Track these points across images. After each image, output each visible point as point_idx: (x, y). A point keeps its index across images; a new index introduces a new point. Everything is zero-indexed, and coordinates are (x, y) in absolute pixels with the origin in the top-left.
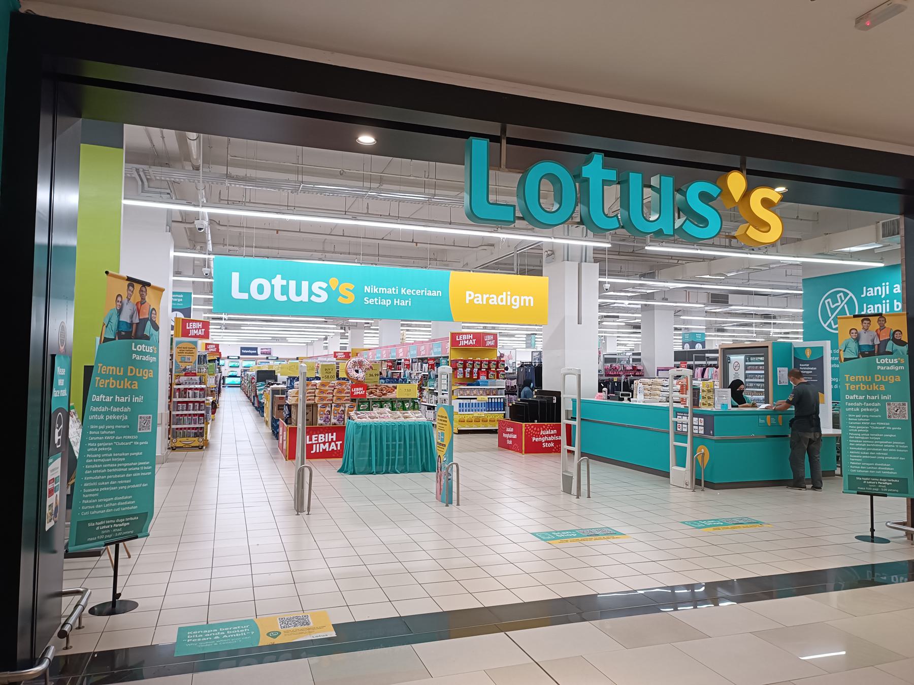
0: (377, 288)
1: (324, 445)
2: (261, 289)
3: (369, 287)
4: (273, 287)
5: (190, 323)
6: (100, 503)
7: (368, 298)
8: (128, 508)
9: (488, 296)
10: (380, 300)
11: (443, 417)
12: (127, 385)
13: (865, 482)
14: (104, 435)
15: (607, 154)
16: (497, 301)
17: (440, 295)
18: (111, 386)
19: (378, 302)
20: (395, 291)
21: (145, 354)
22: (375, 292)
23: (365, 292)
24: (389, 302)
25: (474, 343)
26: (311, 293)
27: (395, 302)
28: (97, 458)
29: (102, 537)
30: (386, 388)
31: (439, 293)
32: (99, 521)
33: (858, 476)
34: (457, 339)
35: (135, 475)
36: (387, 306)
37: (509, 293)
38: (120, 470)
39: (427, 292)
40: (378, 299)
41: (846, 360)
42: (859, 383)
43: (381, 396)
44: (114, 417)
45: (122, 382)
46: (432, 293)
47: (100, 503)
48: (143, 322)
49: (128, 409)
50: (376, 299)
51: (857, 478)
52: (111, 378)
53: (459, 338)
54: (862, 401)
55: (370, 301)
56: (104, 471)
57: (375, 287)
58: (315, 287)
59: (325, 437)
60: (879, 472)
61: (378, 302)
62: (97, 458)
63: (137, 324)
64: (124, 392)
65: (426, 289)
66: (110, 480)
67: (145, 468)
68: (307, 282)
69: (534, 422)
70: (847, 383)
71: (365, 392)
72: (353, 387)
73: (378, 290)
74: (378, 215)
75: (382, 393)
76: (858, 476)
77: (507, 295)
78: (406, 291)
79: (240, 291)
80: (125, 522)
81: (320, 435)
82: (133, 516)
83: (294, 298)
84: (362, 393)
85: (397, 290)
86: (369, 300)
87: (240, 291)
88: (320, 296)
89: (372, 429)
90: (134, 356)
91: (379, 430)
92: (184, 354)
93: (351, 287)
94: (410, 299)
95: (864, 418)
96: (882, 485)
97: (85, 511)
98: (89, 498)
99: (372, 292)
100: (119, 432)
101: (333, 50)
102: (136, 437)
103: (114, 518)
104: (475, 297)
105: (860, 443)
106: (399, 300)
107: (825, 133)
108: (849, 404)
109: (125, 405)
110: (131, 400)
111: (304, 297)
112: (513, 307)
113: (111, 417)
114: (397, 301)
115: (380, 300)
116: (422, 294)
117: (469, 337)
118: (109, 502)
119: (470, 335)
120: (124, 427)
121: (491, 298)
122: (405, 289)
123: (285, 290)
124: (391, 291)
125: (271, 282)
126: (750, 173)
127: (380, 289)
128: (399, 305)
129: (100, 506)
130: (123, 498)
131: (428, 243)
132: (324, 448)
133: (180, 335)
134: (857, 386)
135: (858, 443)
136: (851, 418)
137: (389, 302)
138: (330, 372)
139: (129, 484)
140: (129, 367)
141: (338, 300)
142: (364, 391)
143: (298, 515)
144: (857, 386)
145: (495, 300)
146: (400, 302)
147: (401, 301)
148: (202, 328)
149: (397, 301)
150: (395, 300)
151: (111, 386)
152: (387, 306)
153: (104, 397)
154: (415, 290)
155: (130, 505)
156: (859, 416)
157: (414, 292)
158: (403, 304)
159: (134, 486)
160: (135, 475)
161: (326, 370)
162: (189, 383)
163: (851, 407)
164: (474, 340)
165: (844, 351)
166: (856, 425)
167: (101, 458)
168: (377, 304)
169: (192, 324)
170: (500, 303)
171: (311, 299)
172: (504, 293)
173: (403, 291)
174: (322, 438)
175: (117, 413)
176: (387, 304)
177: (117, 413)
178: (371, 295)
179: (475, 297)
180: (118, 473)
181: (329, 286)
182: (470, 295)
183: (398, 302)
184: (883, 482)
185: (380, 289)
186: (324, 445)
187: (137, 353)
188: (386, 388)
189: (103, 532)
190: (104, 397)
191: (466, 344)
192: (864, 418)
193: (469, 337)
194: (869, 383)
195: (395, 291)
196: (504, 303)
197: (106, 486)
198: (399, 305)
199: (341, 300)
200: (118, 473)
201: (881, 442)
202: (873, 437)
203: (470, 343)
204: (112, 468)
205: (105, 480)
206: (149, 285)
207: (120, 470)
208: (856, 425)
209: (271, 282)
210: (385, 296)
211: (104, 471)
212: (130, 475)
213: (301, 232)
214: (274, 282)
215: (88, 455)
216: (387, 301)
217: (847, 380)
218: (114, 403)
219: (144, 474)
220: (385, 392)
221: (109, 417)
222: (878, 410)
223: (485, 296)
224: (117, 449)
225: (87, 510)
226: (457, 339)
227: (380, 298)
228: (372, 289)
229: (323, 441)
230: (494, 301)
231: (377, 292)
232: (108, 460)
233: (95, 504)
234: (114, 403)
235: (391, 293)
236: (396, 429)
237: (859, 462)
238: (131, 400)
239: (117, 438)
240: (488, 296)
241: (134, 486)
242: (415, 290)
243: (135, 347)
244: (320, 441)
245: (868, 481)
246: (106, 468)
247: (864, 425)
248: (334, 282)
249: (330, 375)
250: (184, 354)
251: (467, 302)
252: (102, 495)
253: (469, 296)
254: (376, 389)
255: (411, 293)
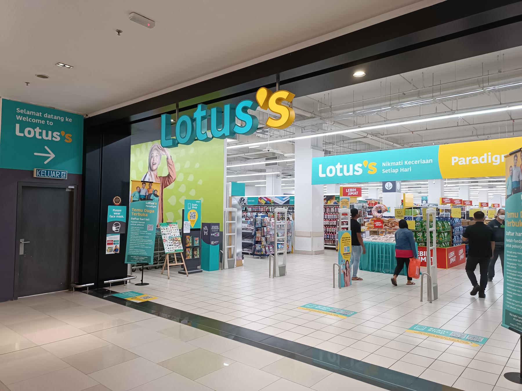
0: (390, 163)
1: (423, 258)
2: (331, 171)
3: (385, 163)
4: (336, 169)
5: (348, 189)
6: (135, 251)
7: (384, 170)
8: (144, 254)
9: (470, 158)
10: (391, 170)
11: (348, 238)
12: (144, 215)
13: (134, 258)
14: (137, 230)
15: (203, 103)
16: (479, 161)
17: (432, 162)
18: (138, 215)
19: (390, 171)
20: (401, 163)
21: (151, 205)
22: (388, 166)
23: (383, 166)
24: (397, 171)
25: (357, 194)
26: (354, 170)
27: (401, 170)
28: (134, 237)
29: (136, 261)
30: (394, 223)
31: (431, 161)
32: (134, 256)
33: (131, 255)
34: (347, 191)
35: (146, 244)
36: (396, 173)
37: (490, 154)
38: (141, 241)
39: (422, 161)
40: (391, 169)
41: (133, 201)
42: (137, 212)
43: (391, 228)
44: (516, 247)
45: (518, 222)
46: (425, 161)
47: (135, 251)
48: (150, 195)
49: (144, 223)
50: (389, 170)
51: (131, 256)
52: (513, 220)
53: (347, 191)
54: (138, 221)
55: (386, 171)
56: (136, 241)
57: (388, 162)
58: (356, 168)
59: (423, 253)
60: (140, 254)
61: (390, 171)
62: (134, 237)
63: (148, 195)
64: (143, 217)
65: (421, 159)
66: (138, 244)
67: (150, 242)
68: (352, 165)
69: (453, 246)
70: (133, 212)
71: (382, 225)
72: (375, 221)
73: (390, 164)
74: (444, 112)
75: (392, 225)
76: (131, 255)
77: (488, 156)
78: (408, 163)
79: (322, 173)
80: (143, 258)
81: (420, 252)
82: (146, 257)
83: (346, 174)
84: (380, 225)
85: (402, 162)
86: (385, 171)
87: (322, 173)
88: (358, 171)
89: (370, 246)
90: (146, 206)
91: (374, 246)
92: (344, 205)
93: (360, 165)
94: (410, 167)
95: (137, 229)
96: (141, 259)
97: (130, 252)
98: (131, 249)
99: (387, 166)
100: (141, 230)
101: (132, 99)
102: (147, 232)
103: (140, 256)
104: (459, 160)
105: (135, 240)
106: (403, 168)
107: (328, 34)
108: (132, 222)
109: (143, 221)
110: (145, 220)
111: (351, 173)
112: (494, 164)
113: (138, 225)
114: (402, 169)
115: (391, 170)
116: (418, 163)
117: (354, 190)
118: (137, 251)
119: (355, 189)
120: (143, 228)
121: (473, 159)
122: (407, 161)
123: (342, 170)
124: (398, 164)
125: (335, 167)
126: (267, 87)
127: (391, 163)
128: (403, 171)
129: (134, 251)
130: (142, 250)
131: (505, 120)
132: (423, 260)
133: (342, 195)
134: (137, 214)
135: (133, 240)
136: (132, 228)
137: (397, 171)
138: (400, 214)
139: (144, 246)
140: (145, 209)
141: (368, 173)
142: (381, 224)
143: (273, 278)
144: (137, 214)
145: (477, 160)
146: (404, 170)
147: (405, 169)
148: (356, 191)
149: (402, 169)
150: (401, 168)
151: (138, 215)
152: (396, 173)
153: (510, 233)
154: (414, 161)
155: (145, 253)
156: (136, 228)
157: (413, 162)
158: (394, 171)
159: (146, 247)
160: (146, 244)
161: (397, 212)
162: (345, 219)
163: (133, 223)
164: (357, 192)
165: (133, 197)
166: (134, 232)
167: (135, 237)
168: (390, 172)
169: (350, 190)
170: (482, 162)
171: (354, 173)
172: (485, 155)
173: (406, 163)
174: (421, 254)
175: (140, 224)
176: (396, 172)
177: (140, 224)
178: (387, 168)
179: (459, 160)
180: (140, 242)
181: (363, 165)
182: (455, 159)
183: (403, 170)
184: (141, 258)
185: (391, 163)
186: (423, 258)
187: (147, 205)
188: (394, 223)
189: (136, 260)
190: (510, 233)
191: (352, 195)
192: (137, 229)
193: (354, 190)
194: (142, 213)
195: (401, 163)
196: (485, 161)
197: (137, 246)
198: (403, 171)
199: (370, 172)
200: (140, 242)
201: (143, 240)
202: (140, 237)
203: (355, 194)
204: (138, 240)
205: (136, 244)
206: (153, 182)
207: (141, 241)
208: (134, 232)
209: (335, 167)
210: (394, 167)
211: (136, 241)
212: (144, 243)
213: (459, 126)
214: (337, 167)
215: (131, 236)
216: (396, 170)
217: (133, 211)
218: (139, 220)
219: (150, 244)
220: (394, 225)
221: (138, 225)
222: (143, 225)
223: (468, 159)
224: (140, 235)
225: (131, 252)
226: (347, 191)
227: (391, 169)
228: (387, 163)
229: (423, 255)
230: (476, 161)
231: (390, 165)
232: (137, 238)
233: (133, 250)
234: (139, 220)
235: (398, 165)
236: (384, 247)
237: (132, 249)
238: (145, 220)
239: (140, 231)
240: (470, 158)
241: (146, 247)
242: (414, 161)
243: (147, 203)
244: (420, 255)
245: (136, 257)
246: (137, 240)
247: (137, 232)
248: (366, 162)
249: (400, 215)
250: (344, 205)
251: (453, 164)
252: (135, 248)
253: (454, 160)
254: (388, 223)
255: (411, 163)
